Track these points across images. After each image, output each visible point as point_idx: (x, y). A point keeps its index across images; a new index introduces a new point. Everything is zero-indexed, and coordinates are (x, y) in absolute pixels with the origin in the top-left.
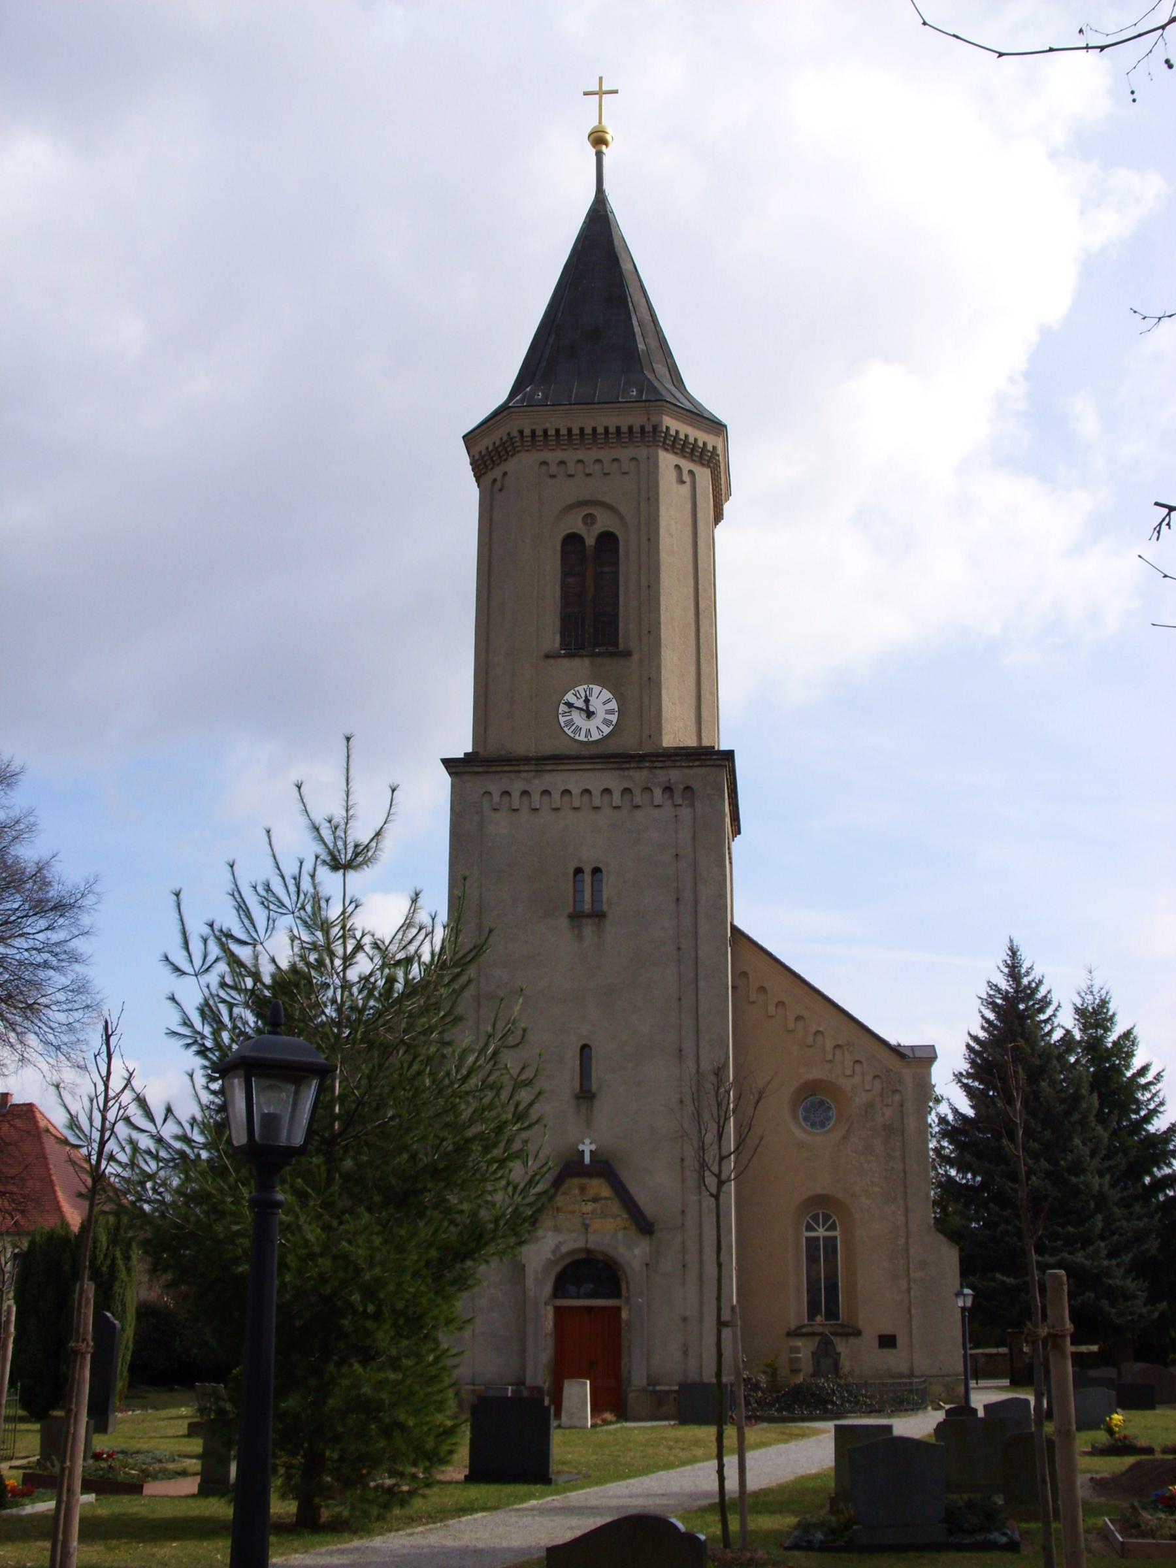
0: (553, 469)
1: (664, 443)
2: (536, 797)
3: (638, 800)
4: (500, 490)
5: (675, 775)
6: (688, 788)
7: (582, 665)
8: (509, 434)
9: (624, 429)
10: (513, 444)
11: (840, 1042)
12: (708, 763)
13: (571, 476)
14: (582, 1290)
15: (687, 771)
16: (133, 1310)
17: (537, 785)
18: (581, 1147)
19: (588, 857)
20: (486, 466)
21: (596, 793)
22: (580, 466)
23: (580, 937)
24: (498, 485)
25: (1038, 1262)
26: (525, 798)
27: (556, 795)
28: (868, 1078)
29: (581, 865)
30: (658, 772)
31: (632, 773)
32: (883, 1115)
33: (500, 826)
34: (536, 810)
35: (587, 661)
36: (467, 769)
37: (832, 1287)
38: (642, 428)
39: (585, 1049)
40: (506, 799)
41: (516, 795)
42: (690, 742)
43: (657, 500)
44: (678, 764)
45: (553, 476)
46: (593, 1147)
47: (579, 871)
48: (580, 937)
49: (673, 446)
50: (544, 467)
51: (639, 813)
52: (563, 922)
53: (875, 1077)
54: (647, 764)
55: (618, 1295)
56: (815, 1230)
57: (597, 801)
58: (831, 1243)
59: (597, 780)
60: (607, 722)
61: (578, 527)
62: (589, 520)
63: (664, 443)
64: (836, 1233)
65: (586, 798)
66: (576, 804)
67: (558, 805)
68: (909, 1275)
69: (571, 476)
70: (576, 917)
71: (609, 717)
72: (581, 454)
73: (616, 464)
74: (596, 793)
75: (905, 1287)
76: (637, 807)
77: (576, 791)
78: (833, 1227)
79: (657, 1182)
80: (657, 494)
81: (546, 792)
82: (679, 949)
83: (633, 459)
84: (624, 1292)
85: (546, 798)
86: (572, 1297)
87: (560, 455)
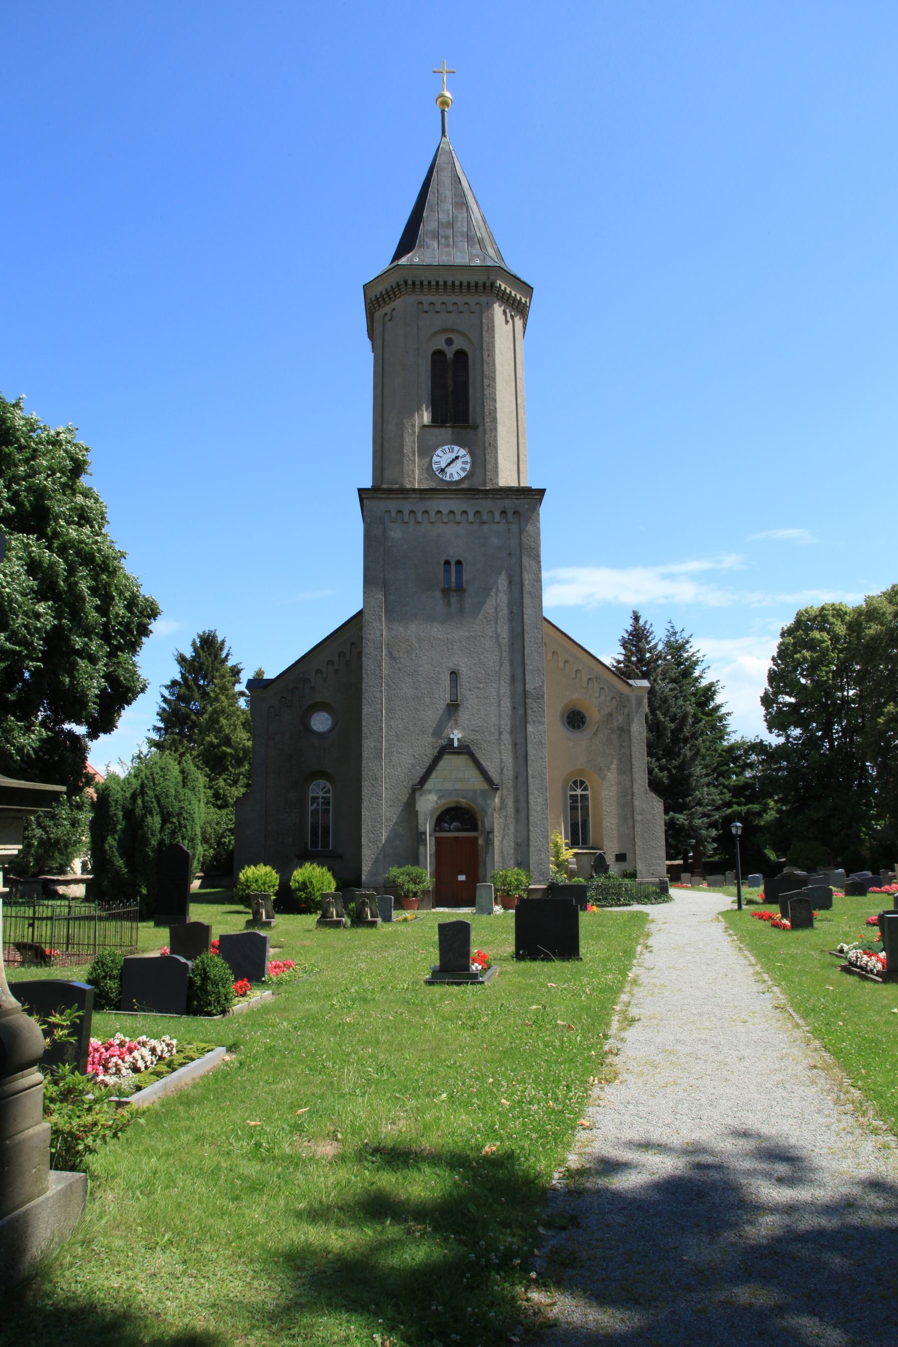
0: (426, 307)
2: (419, 515)
3: (485, 518)
4: (390, 320)
13: (438, 312)
14: (452, 827)
15: (516, 501)
17: (407, 507)
18: (452, 736)
19: (454, 552)
21: (458, 513)
22: (443, 306)
23: (448, 604)
24: (388, 317)
26: (412, 515)
27: (432, 514)
28: (609, 699)
29: (449, 559)
30: (498, 501)
31: (480, 501)
33: (396, 533)
34: (419, 523)
35: (449, 430)
37: (585, 824)
38: (484, 284)
39: (454, 674)
41: (406, 513)
42: (514, 484)
43: (493, 330)
46: (460, 736)
48: (448, 604)
50: (420, 306)
52: (438, 594)
55: (475, 828)
57: (458, 519)
58: (584, 798)
62: (449, 342)
67: (433, 520)
69: (438, 312)
71: (464, 466)
72: (444, 298)
73: (466, 306)
74: (458, 513)
75: (631, 825)
76: (484, 523)
78: (585, 789)
79: (498, 759)
81: (425, 512)
82: (512, 612)
84: (480, 827)
85: (426, 516)
86: (446, 831)
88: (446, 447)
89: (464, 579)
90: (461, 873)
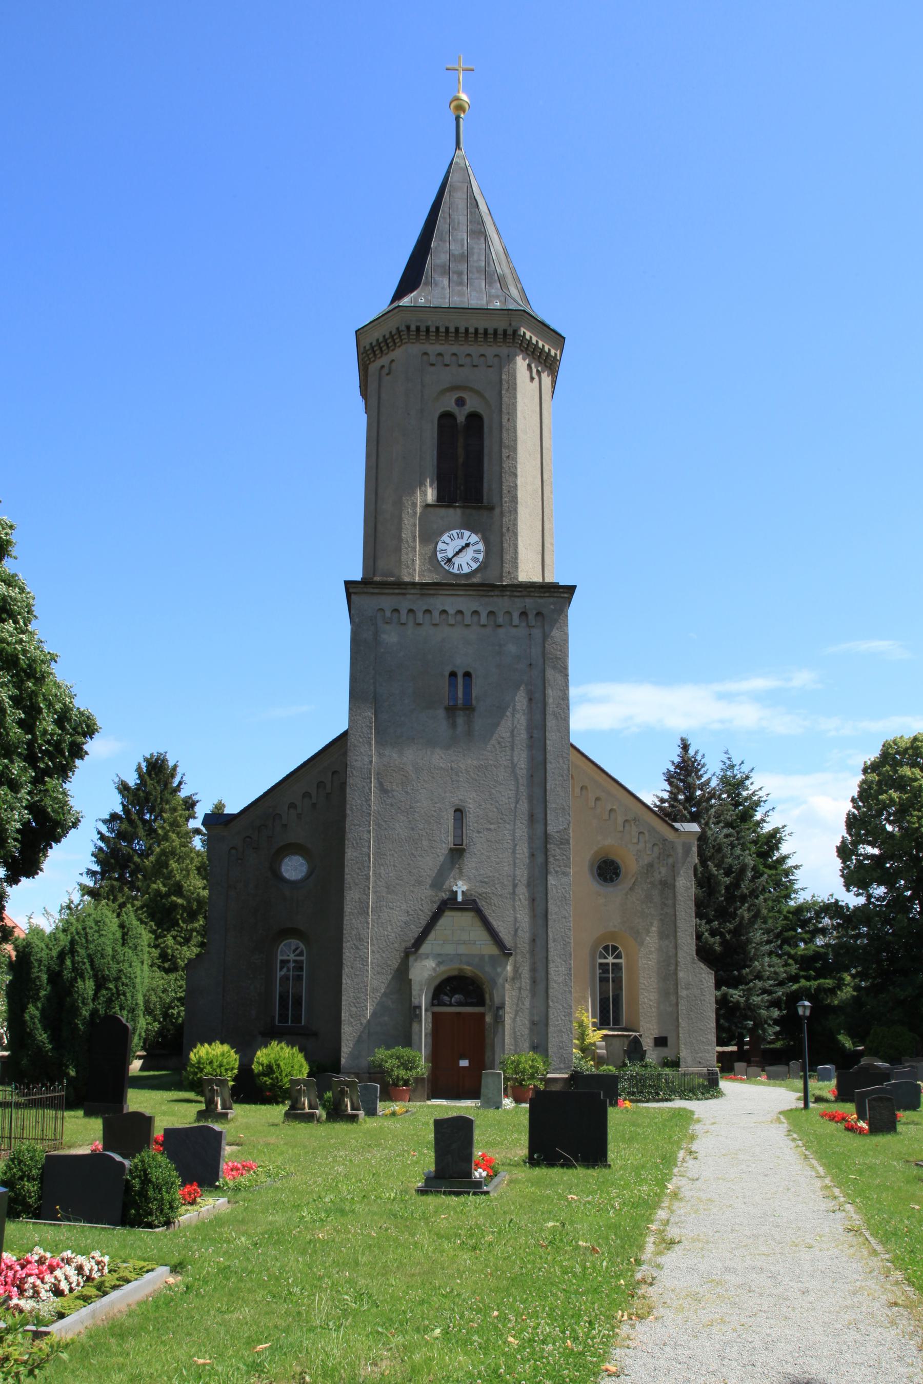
0: (433, 359)
1: (521, 345)
2: (420, 615)
3: (500, 620)
4: (388, 374)
5: (529, 603)
6: (539, 614)
7: (454, 514)
8: (398, 329)
9: (491, 331)
10: (400, 336)
11: (628, 818)
12: (556, 595)
13: (447, 365)
16: (820, 1083)
18: (455, 888)
19: (461, 663)
20: (369, 359)
21: (468, 614)
23: (454, 725)
24: (386, 370)
25: (302, 970)
27: (436, 614)
29: (455, 670)
30: (517, 600)
31: (495, 599)
32: (660, 873)
33: (391, 637)
34: (419, 624)
35: (459, 511)
36: (365, 590)
38: (505, 331)
39: (459, 812)
40: (396, 615)
41: (404, 612)
42: (537, 578)
44: (532, 594)
45: (432, 365)
46: (465, 888)
47: (453, 675)
48: (454, 725)
49: (527, 349)
50: (425, 357)
51: (501, 631)
52: (441, 713)
53: (654, 845)
54: (508, 593)
55: (481, 1002)
56: (605, 958)
57: (468, 620)
58: (617, 967)
59: (466, 603)
60: (475, 560)
61: (451, 406)
62: (460, 402)
63: (521, 345)
64: (303, 958)
65: (459, 617)
66: (452, 621)
67: (437, 622)
68: (677, 993)
69: (447, 365)
70: (451, 710)
72: (455, 349)
73: (483, 359)
74: (468, 614)
76: (500, 626)
77: (451, 611)
78: (618, 956)
80: (515, 384)
81: (427, 611)
82: (532, 737)
83: (496, 356)
84: (488, 1001)
86: (445, 1005)
87: (438, 348)
88: (454, 532)
89: (474, 695)
90: (463, 1057)
